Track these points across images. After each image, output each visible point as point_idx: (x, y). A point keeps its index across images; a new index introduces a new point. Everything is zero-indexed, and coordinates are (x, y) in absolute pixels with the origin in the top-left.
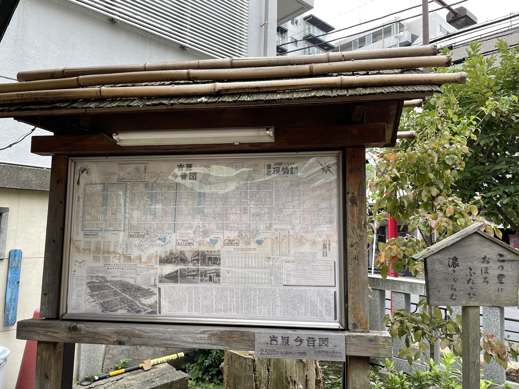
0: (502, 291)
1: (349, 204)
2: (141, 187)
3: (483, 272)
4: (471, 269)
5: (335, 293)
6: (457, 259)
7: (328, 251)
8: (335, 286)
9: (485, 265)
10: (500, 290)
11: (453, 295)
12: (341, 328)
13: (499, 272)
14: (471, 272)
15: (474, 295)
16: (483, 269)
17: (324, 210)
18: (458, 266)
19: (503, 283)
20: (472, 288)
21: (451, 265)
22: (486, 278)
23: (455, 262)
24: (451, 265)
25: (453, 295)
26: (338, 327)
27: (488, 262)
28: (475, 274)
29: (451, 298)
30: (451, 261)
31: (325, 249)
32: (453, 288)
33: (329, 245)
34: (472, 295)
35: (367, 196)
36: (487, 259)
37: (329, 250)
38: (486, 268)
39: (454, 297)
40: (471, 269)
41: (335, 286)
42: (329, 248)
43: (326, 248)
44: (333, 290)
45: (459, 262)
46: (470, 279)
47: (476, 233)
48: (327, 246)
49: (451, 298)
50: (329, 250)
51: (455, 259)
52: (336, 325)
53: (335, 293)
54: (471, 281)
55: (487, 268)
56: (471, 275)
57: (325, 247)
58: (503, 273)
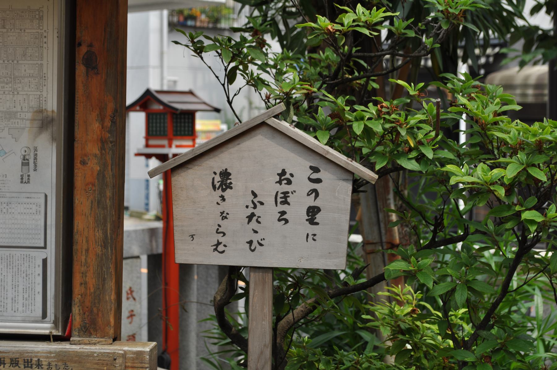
0: (314, 240)
1: (80, 70)
2: (207, 9)
3: (279, 200)
4: (255, 195)
5: (45, 261)
6: (230, 174)
7: (32, 173)
8: (45, 247)
9: (285, 187)
10: (310, 237)
11: (219, 243)
12: (55, 333)
13: (310, 201)
14: (256, 201)
15: (261, 245)
16: (280, 195)
17: (26, 80)
18: (231, 188)
19: (317, 224)
20: (256, 232)
21: (218, 185)
22: (283, 213)
23: (225, 181)
24: (218, 185)
25: (219, 243)
26: (47, 332)
27: (289, 182)
28: (262, 203)
29: (216, 250)
30: (218, 178)
31: (25, 168)
32: (221, 230)
33: (35, 159)
34: (255, 244)
35: (337, 65)
36: (288, 176)
37: (35, 170)
38: (286, 194)
39: (221, 248)
40: (255, 195)
41: (45, 247)
42: (35, 166)
43: (28, 164)
44: (40, 255)
45: (233, 179)
46: (253, 215)
47: (263, 124)
48: (31, 162)
49: (216, 250)
50: (35, 170)
51: (225, 175)
52: (45, 328)
53: (45, 261)
54: (255, 218)
55: (288, 193)
56: (255, 207)
57: (25, 163)
58: (317, 203)
